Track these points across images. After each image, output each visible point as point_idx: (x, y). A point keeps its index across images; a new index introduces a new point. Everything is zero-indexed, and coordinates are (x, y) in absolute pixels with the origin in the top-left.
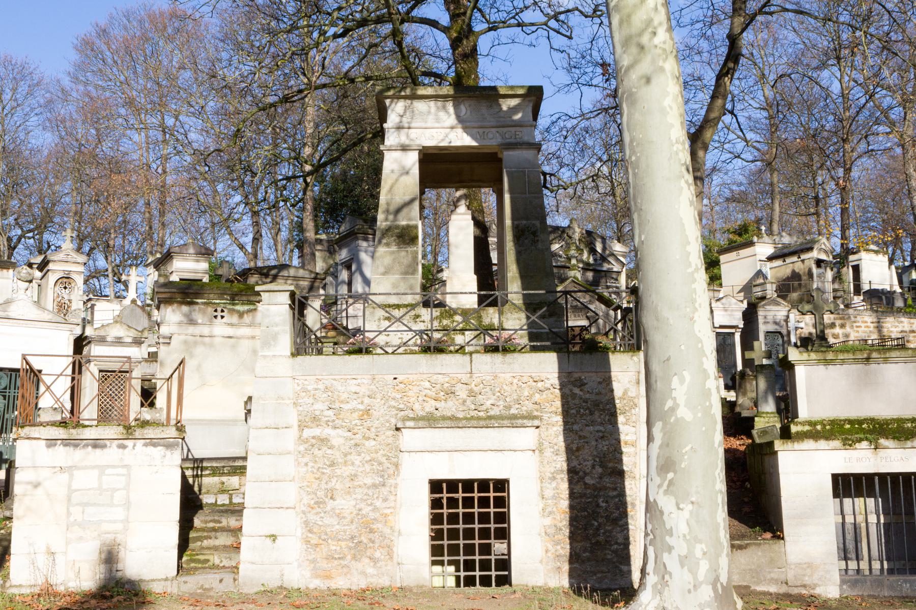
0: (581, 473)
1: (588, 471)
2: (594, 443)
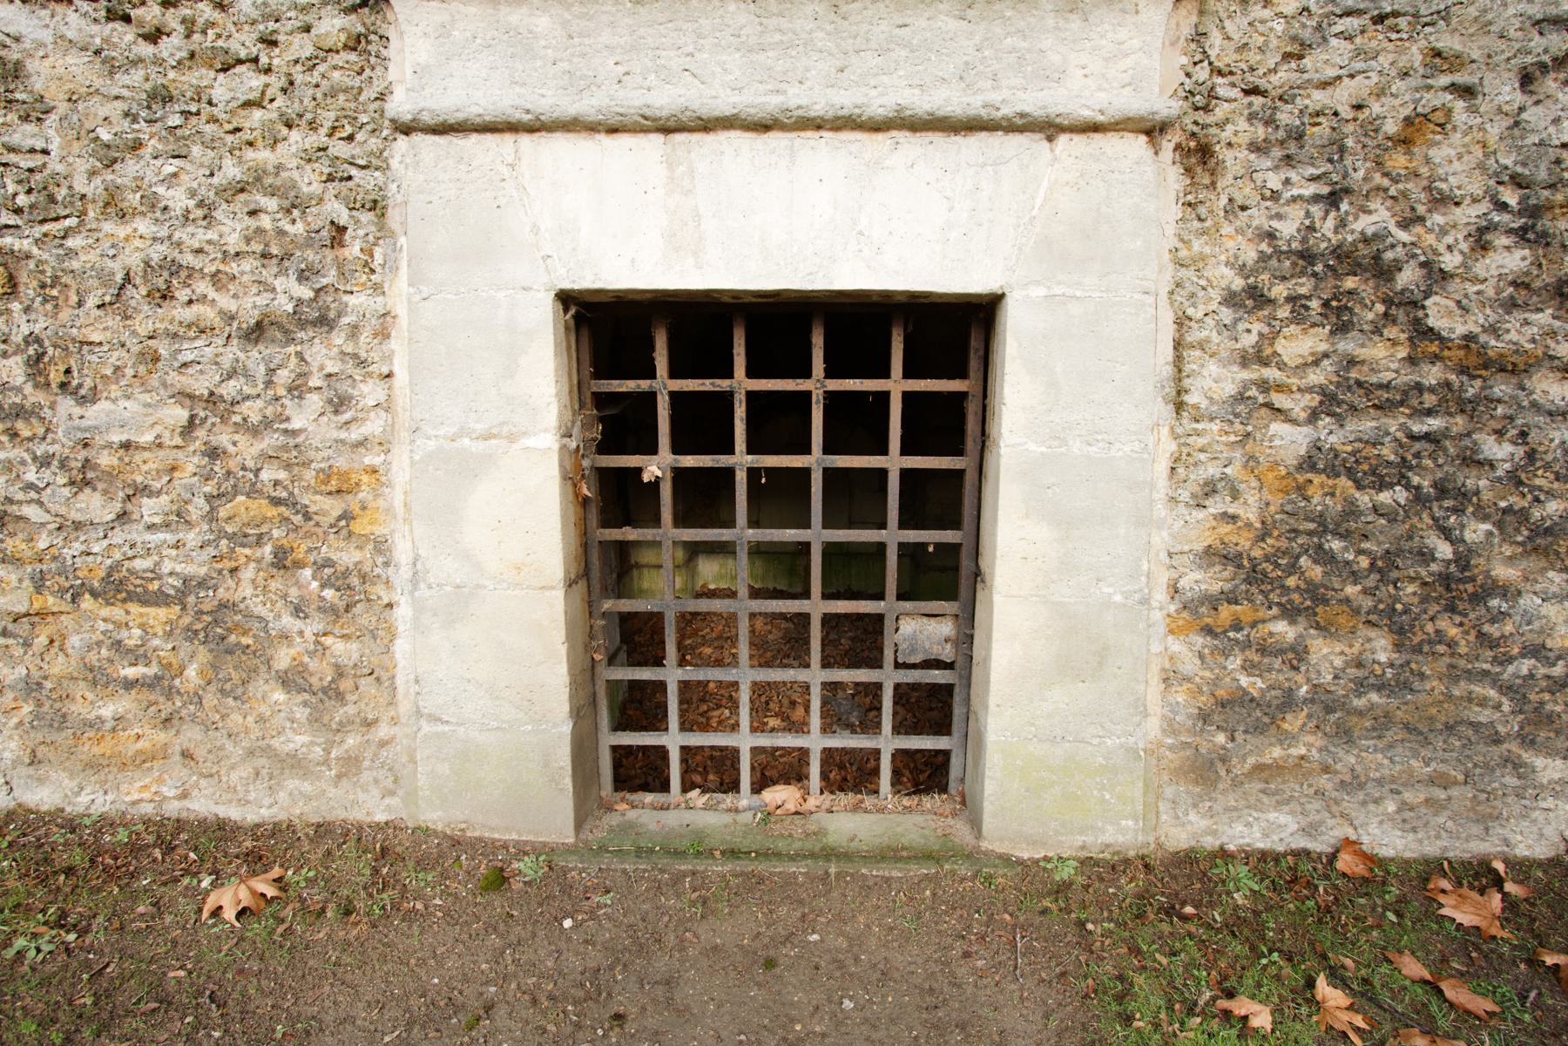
0: (1408, 277)
1: (1450, 261)
2: (1506, 92)
